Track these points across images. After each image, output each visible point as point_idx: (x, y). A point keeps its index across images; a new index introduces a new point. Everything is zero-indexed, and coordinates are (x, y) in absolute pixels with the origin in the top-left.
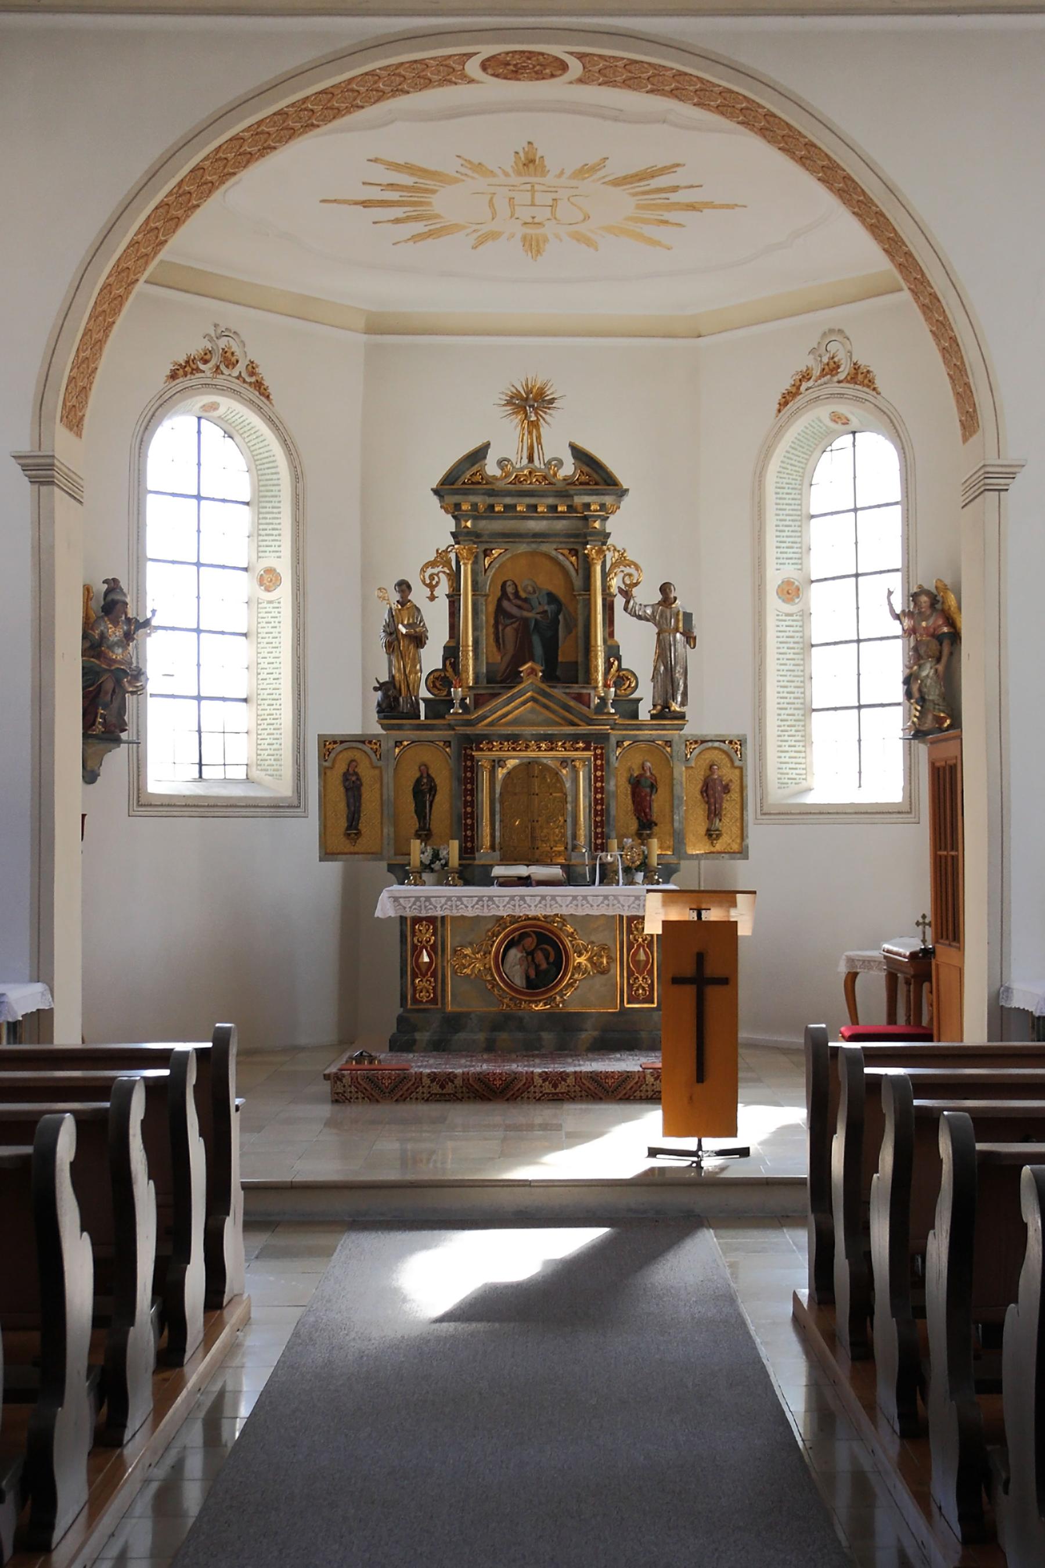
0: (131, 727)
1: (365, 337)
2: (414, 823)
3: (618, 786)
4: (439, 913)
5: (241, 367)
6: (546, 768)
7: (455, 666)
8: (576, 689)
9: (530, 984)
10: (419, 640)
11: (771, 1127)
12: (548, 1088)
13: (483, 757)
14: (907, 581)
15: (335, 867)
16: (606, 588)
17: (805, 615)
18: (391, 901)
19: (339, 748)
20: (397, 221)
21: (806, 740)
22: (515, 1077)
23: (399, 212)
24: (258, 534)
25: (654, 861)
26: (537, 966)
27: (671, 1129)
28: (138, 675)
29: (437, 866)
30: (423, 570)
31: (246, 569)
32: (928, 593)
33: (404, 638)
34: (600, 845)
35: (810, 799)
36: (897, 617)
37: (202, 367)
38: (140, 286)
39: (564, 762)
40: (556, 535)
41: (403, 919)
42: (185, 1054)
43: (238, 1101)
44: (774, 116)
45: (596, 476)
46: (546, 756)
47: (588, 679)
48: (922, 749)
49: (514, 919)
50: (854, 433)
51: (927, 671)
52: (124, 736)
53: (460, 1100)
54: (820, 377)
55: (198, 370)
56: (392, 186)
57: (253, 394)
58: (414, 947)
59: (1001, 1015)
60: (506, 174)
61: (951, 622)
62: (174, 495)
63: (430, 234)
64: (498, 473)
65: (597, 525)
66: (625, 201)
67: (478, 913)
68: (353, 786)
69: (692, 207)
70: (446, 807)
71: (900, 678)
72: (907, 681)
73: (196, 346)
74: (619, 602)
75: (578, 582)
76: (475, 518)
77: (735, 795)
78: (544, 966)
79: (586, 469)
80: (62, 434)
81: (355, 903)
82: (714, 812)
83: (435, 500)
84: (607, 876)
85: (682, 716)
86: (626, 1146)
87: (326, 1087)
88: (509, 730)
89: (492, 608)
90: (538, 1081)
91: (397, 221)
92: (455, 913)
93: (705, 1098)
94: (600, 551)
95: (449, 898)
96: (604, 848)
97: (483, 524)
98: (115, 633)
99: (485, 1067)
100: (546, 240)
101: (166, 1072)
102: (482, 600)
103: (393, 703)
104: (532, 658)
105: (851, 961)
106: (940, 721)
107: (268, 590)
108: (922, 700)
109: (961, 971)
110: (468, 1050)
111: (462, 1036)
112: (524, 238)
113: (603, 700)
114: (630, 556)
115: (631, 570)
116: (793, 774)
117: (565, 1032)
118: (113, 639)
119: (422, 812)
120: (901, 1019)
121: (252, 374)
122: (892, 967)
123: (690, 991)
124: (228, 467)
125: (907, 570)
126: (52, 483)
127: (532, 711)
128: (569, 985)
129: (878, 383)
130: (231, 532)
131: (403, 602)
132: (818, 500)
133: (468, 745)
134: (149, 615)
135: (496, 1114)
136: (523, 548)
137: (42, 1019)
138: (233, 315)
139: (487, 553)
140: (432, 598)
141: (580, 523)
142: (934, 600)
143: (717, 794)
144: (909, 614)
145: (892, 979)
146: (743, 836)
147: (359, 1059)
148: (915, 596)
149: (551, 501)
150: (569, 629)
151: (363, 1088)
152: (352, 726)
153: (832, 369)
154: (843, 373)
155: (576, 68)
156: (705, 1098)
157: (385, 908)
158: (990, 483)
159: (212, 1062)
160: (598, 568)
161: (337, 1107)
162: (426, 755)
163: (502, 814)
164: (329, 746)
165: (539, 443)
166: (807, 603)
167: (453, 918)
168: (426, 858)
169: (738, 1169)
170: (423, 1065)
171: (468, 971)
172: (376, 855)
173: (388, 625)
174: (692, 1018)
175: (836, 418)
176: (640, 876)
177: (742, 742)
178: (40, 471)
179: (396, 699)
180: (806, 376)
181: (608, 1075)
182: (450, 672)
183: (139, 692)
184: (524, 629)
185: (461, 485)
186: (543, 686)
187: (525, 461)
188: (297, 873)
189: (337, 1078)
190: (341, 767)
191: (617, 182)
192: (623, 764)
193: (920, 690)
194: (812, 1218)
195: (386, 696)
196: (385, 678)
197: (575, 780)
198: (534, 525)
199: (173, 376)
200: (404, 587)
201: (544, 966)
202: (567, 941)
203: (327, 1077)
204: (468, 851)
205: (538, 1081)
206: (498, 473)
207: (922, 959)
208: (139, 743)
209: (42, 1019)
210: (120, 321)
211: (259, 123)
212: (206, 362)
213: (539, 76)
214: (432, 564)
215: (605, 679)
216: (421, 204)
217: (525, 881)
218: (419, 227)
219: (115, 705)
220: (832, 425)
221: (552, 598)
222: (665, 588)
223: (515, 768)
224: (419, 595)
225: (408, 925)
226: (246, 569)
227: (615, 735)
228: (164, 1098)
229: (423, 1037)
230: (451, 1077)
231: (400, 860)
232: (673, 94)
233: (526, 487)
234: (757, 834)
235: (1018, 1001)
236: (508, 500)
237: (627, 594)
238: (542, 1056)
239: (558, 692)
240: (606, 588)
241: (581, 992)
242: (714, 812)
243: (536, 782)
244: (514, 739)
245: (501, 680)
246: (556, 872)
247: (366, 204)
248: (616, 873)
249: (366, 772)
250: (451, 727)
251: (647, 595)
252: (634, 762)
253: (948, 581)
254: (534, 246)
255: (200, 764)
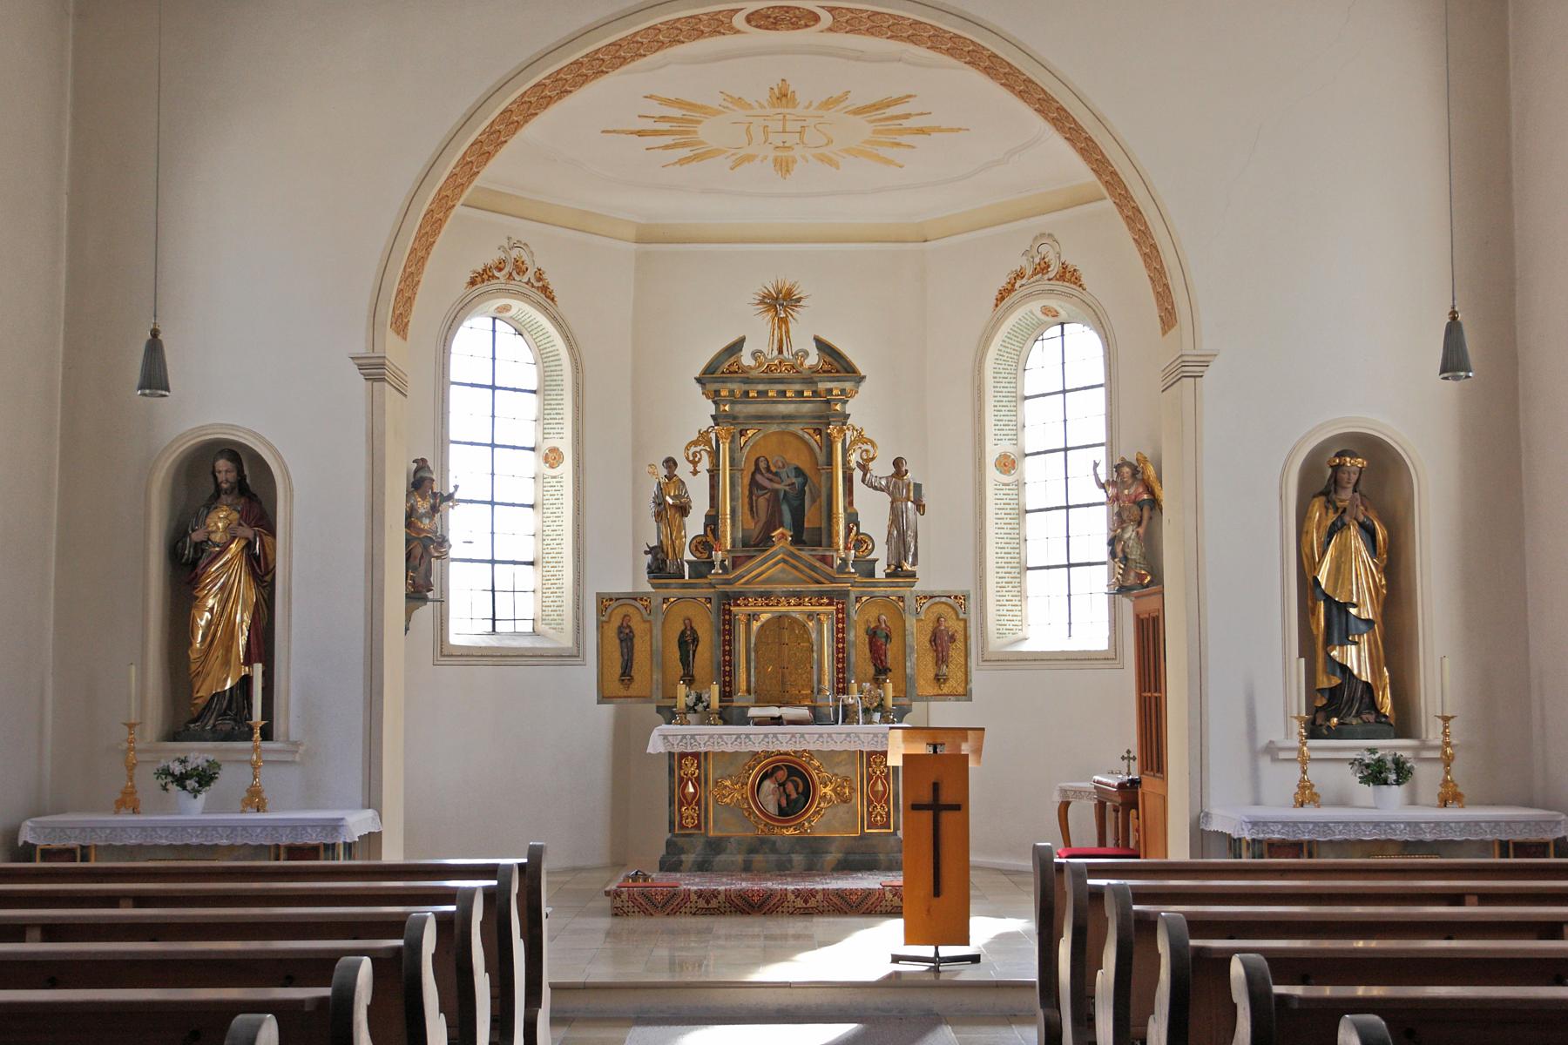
0: (436, 588)
1: (635, 246)
2: (679, 670)
3: (857, 636)
4: (703, 749)
5: (530, 274)
6: (795, 620)
7: (715, 532)
8: (820, 551)
9: (782, 812)
10: (683, 510)
11: (1000, 934)
12: (800, 903)
13: (740, 611)
14: (1110, 454)
15: (608, 709)
16: (846, 463)
17: (1020, 485)
18: (661, 739)
19: (614, 604)
20: (667, 147)
21: (1022, 595)
22: (770, 894)
23: (668, 140)
24: (544, 419)
25: (890, 702)
26: (788, 796)
27: (910, 939)
28: (443, 542)
29: (700, 707)
30: (687, 448)
31: (533, 449)
32: (1130, 465)
33: (671, 509)
34: (842, 688)
35: (1025, 647)
36: (1102, 486)
37: (497, 274)
38: (459, 209)
39: (810, 616)
40: (802, 417)
41: (671, 755)
42: (510, 867)
43: (548, 910)
44: (996, 56)
45: (837, 364)
46: (796, 611)
47: (831, 544)
48: (1127, 604)
49: (768, 754)
50: (1062, 324)
51: (1130, 533)
52: (430, 595)
53: (724, 914)
54: (736, 11)
55: (494, 277)
56: (663, 118)
57: (540, 297)
58: (681, 779)
59: (1200, 836)
60: (762, 107)
61: (1150, 490)
62: (472, 385)
63: (696, 158)
64: (752, 363)
65: (838, 407)
66: (864, 127)
67: (737, 749)
68: (626, 638)
69: (921, 131)
70: (707, 655)
71: (1105, 540)
72: (1112, 542)
73: (492, 257)
74: (857, 475)
75: (821, 458)
76: (733, 403)
77: (960, 644)
78: (794, 796)
79: (828, 359)
80: (391, 337)
81: (626, 742)
82: (941, 659)
83: (698, 388)
84: (848, 716)
85: (913, 575)
86: (870, 951)
87: (606, 903)
88: (763, 588)
89: (747, 481)
90: (791, 897)
91: (667, 147)
92: (717, 749)
93: (939, 909)
94: (841, 431)
95: (711, 736)
96: (845, 691)
97: (738, 407)
98: (423, 506)
99: (744, 884)
100: (794, 161)
101: (495, 883)
102: (738, 474)
103: (661, 565)
104: (781, 525)
105: (1064, 791)
106: (1141, 577)
107: (552, 467)
108: (1125, 559)
109: (1165, 799)
110: (727, 870)
111: (722, 857)
112: (775, 160)
113: (844, 561)
114: (866, 434)
115: (868, 447)
116: (1010, 625)
117: (813, 855)
118: (422, 511)
119: (686, 661)
120: (1110, 842)
121: (539, 279)
122: (1102, 794)
123: (927, 816)
124: (518, 362)
125: (1110, 445)
126: (383, 380)
127: (783, 571)
128: (817, 812)
129: (1084, 280)
130: (520, 418)
131: (670, 477)
132: (1032, 383)
133: (728, 599)
134: (451, 490)
135: (755, 926)
136: (774, 428)
137: (372, 840)
138: (524, 230)
139: (742, 433)
140: (695, 473)
141: (823, 406)
142: (1135, 471)
143: (940, 643)
144: (1112, 483)
145: (1101, 806)
146: (967, 681)
147: (635, 877)
148: (1118, 468)
149: (798, 387)
150: (813, 501)
151: (639, 903)
152: (625, 587)
153: (1043, 268)
154: (1054, 269)
155: (827, 19)
156: (939, 909)
157: (656, 745)
158: (1186, 370)
159: (530, 873)
160: (839, 446)
161: (617, 920)
162: (690, 610)
163: (757, 662)
164: (606, 602)
165: (788, 337)
166: (1022, 473)
167: (715, 754)
168: (691, 701)
169: (968, 973)
170: (691, 883)
171: (727, 800)
172: (646, 698)
173: (657, 497)
174: (927, 840)
175: (1046, 311)
176: (877, 716)
177: (966, 597)
178: (374, 370)
179: (664, 561)
180: (1020, 275)
181: (852, 892)
182: (710, 538)
183: (443, 556)
184: (775, 500)
185: (719, 374)
186: (792, 549)
187: (776, 352)
188: (579, 714)
189: (617, 894)
190: (616, 622)
191: (858, 111)
192: (860, 618)
193: (1123, 551)
194: (1041, 1014)
195: (655, 558)
196: (654, 543)
197: (820, 632)
198: (783, 409)
199: (473, 283)
200: (670, 463)
201: (794, 796)
202: (814, 773)
203: (607, 893)
204: (726, 695)
205: (791, 897)
206: (752, 363)
207: (1130, 789)
208: (443, 601)
209: (372, 840)
210: (440, 239)
211: (558, 72)
212: (500, 270)
213: (795, 26)
214: (695, 443)
215: (846, 543)
216: (687, 132)
217: (777, 721)
218: (685, 152)
219: (422, 569)
220: (1043, 317)
221: (799, 472)
222: (898, 463)
223: (768, 621)
224: (683, 470)
225: (676, 760)
226: (533, 449)
227: (854, 592)
228: (496, 902)
229: (689, 858)
230: (715, 894)
231: (668, 703)
232: (910, 39)
233: (777, 375)
234: (980, 679)
235: (1215, 826)
236: (761, 387)
237: (864, 468)
238: (794, 876)
239: (805, 554)
240: (846, 463)
241: (827, 819)
242: (941, 659)
243: (786, 633)
244: (766, 596)
245: (757, 543)
246: (804, 712)
247: (640, 133)
248: (856, 713)
249: (637, 625)
250: (712, 585)
251: (882, 469)
252: (872, 614)
253: (1147, 454)
254: (784, 166)
255: (494, 620)
